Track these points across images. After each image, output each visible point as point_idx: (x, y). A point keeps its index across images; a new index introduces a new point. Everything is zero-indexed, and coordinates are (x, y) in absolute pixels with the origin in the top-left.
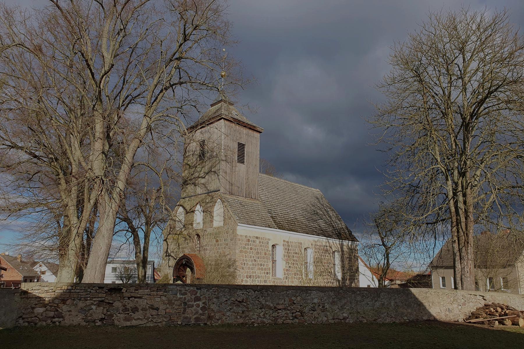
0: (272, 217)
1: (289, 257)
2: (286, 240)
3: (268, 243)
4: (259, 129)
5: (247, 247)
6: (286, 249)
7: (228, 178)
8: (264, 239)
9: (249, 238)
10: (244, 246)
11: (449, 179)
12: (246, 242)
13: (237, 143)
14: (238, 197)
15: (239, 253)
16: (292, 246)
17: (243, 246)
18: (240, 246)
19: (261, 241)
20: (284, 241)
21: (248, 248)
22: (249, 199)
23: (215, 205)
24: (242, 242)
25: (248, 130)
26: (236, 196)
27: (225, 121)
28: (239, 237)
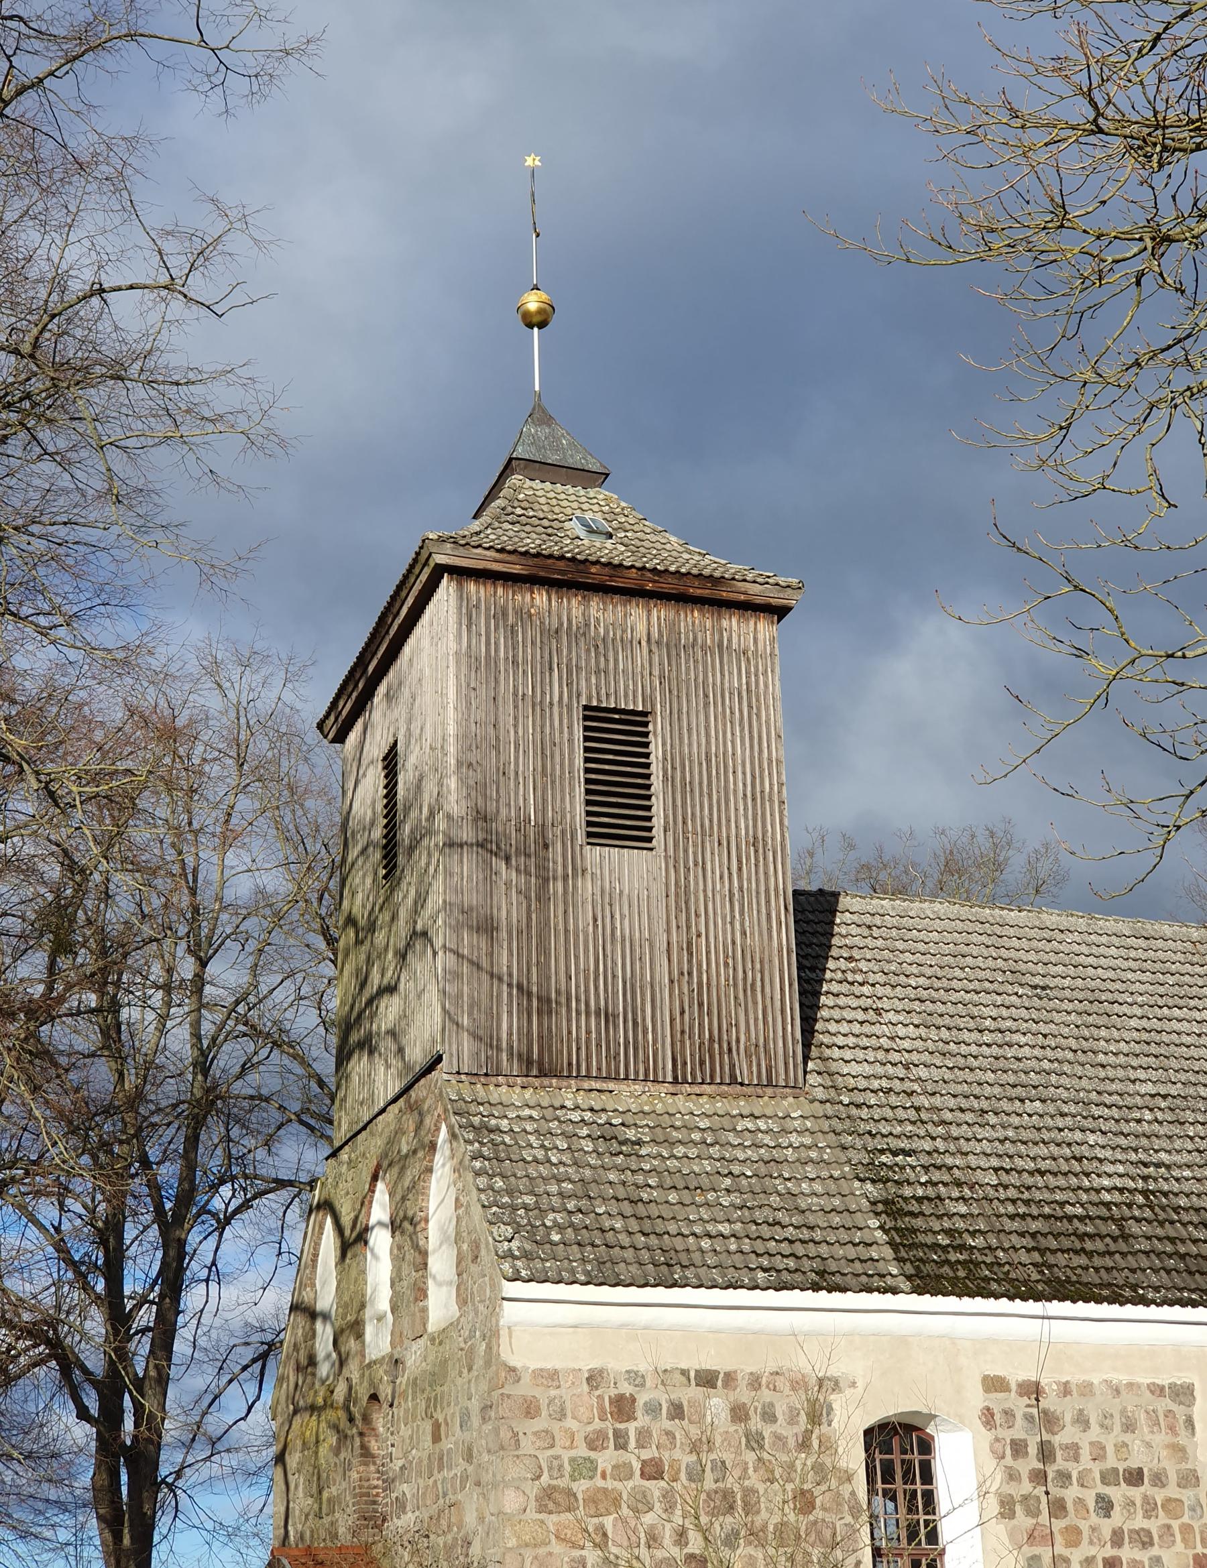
0: (889, 1208)
1: (1058, 1508)
2: (1018, 1374)
3: (817, 1414)
4: (755, 589)
5: (606, 1458)
6: (1018, 1448)
7: (503, 960)
8: (780, 1382)
9: (626, 1389)
10: (582, 1451)
11: (425, 810)
12: (597, 1424)
13: (578, 714)
14: (611, 1085)
15: (532, 1514)
16: (1082, 1421)
17: (566, 1456)
18: (543, 1456)
19: (743, 1394)
20: (994, 1384)
21: (622, 1471)
22: (707, 1089)
23: (430, 1170)
24: (555, 1427)
25: (672, 614)
26: (586, 1085)
27: (471, 587)
28: (526, 1388)
